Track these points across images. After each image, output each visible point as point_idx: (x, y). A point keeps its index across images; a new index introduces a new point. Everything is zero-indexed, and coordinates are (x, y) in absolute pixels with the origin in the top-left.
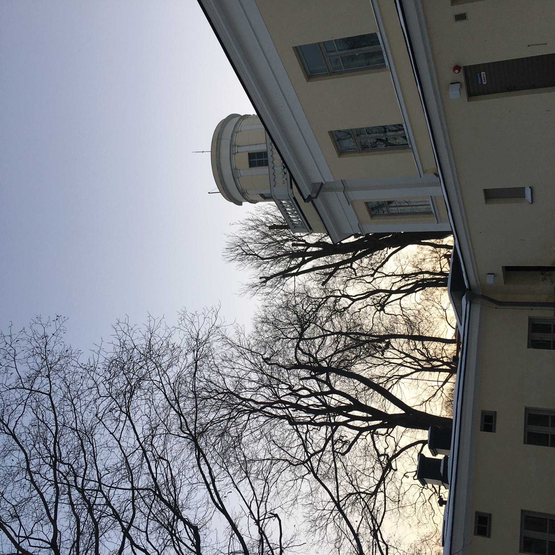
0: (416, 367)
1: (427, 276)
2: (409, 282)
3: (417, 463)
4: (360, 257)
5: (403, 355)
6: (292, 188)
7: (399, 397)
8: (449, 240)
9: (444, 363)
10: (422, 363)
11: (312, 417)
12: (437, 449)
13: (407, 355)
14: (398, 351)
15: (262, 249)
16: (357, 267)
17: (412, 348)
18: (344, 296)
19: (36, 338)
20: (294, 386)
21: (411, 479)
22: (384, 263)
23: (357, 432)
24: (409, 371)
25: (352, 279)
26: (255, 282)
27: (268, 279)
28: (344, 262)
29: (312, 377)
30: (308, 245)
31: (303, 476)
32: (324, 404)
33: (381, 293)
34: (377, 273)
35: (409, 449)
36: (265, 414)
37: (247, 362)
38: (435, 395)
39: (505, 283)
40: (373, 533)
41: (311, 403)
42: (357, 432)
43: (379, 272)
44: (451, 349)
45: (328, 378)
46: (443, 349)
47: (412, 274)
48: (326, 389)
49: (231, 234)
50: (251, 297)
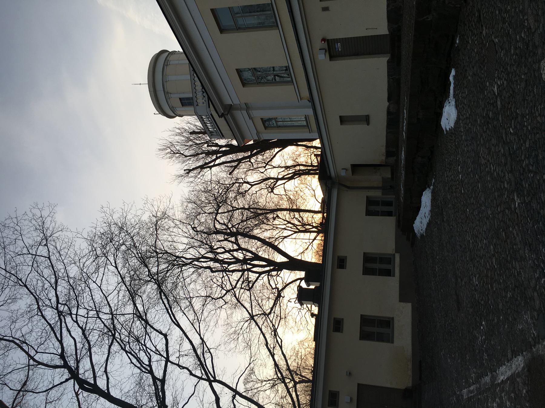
0: (295, 230)
1: (302, 168)
2: (290, 172)
3: (297, 292)
4: (256, 154)
5: (286, 222)
6: (209, 107)
7: (283, 249)
8: (317, 143)
9: (314, 227)
10: (299, 227)
11: (226, 267)
12: (302, 301)
13: (289, 222)
14: (283, 219)
15: (186, 150)
16: (254, 161)
17: (292, 217)
18: (245, 182)
19: (35, 219)
20: (213, 246)
21: (293, 303)
22: (272, 158)
23: (257, 275)
24: (290, 233)
25: (250, 170)
26: (181, 173)
27: (190, 171)
28: (244, 158)
29: (226, 240)
30: (221, 147)
31: (221, 307)
32: (235, 258)
33: (271, 180)
34: (268, 165)
35: (291, 284)
36: (195, 266)
37: (180, 230)
38: (307, 249)
39: (353, 175)
40: (273, 333)
41: (225, 257)
42: (257, 275)
43: (269, 165)
44: (318, 218)
45: (236, 240)
46: (312, 217)
47: (292, 166)
48: (235, 247)
49: (162, 138)
50: (178, 184)
